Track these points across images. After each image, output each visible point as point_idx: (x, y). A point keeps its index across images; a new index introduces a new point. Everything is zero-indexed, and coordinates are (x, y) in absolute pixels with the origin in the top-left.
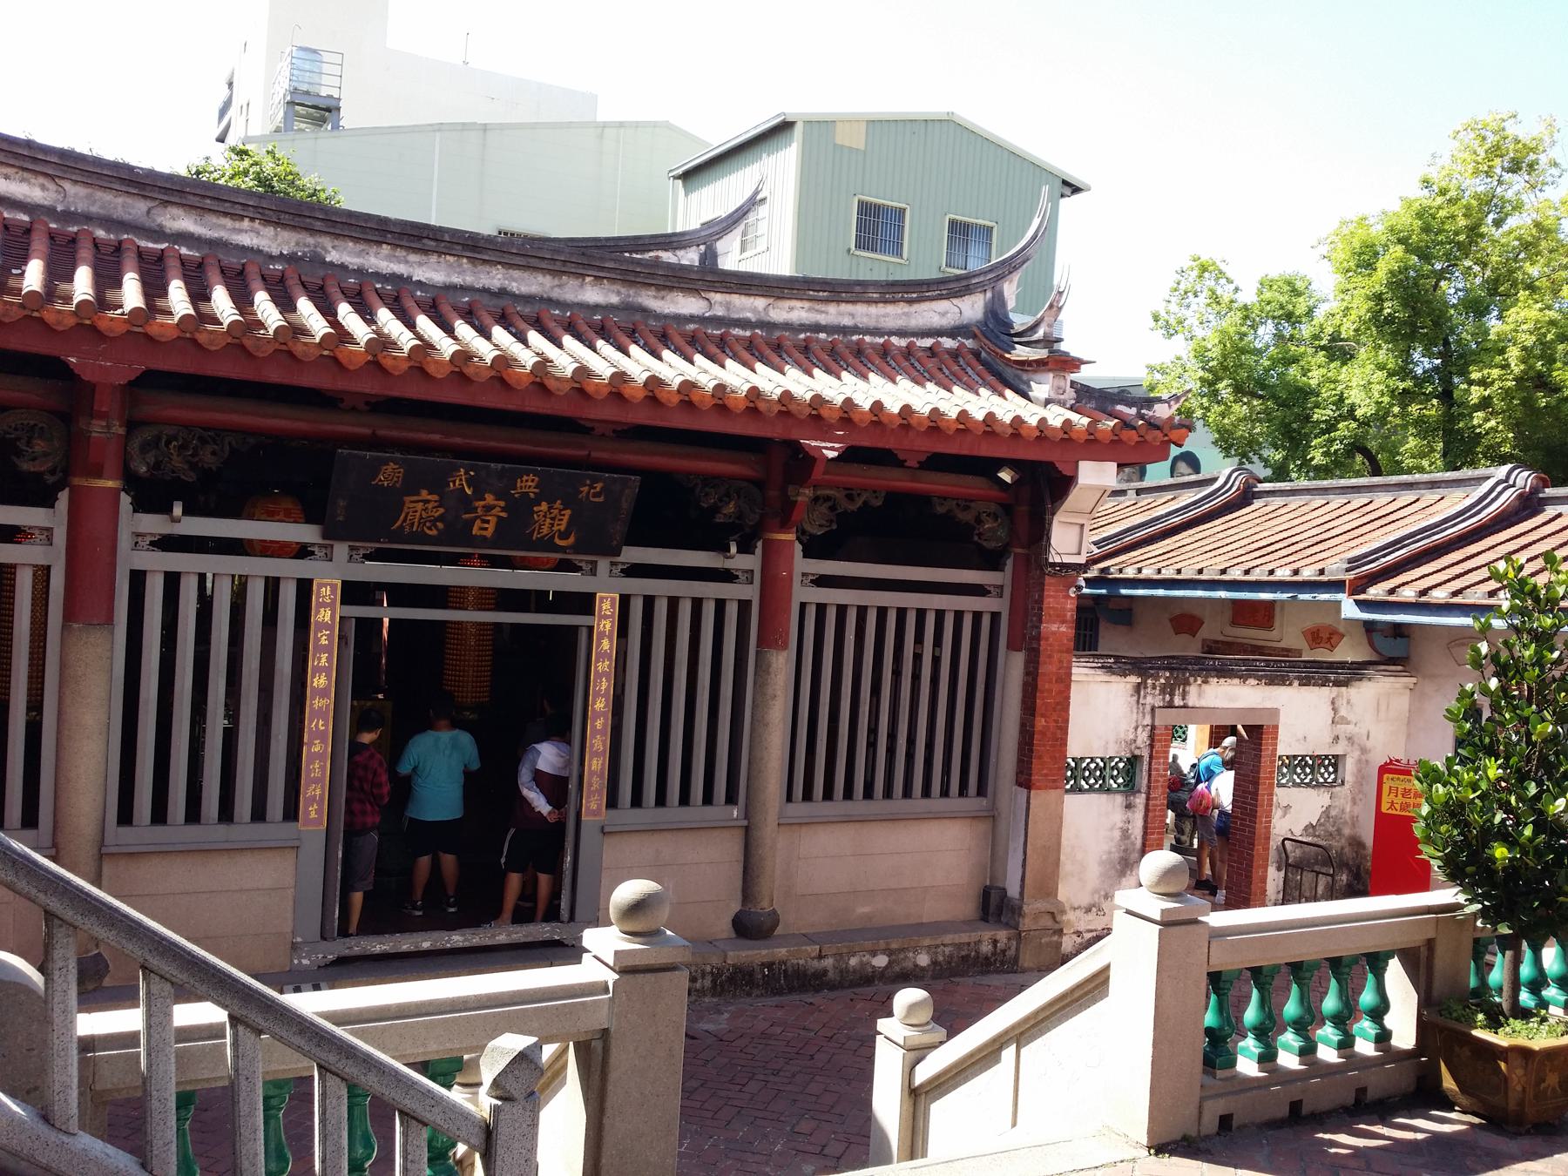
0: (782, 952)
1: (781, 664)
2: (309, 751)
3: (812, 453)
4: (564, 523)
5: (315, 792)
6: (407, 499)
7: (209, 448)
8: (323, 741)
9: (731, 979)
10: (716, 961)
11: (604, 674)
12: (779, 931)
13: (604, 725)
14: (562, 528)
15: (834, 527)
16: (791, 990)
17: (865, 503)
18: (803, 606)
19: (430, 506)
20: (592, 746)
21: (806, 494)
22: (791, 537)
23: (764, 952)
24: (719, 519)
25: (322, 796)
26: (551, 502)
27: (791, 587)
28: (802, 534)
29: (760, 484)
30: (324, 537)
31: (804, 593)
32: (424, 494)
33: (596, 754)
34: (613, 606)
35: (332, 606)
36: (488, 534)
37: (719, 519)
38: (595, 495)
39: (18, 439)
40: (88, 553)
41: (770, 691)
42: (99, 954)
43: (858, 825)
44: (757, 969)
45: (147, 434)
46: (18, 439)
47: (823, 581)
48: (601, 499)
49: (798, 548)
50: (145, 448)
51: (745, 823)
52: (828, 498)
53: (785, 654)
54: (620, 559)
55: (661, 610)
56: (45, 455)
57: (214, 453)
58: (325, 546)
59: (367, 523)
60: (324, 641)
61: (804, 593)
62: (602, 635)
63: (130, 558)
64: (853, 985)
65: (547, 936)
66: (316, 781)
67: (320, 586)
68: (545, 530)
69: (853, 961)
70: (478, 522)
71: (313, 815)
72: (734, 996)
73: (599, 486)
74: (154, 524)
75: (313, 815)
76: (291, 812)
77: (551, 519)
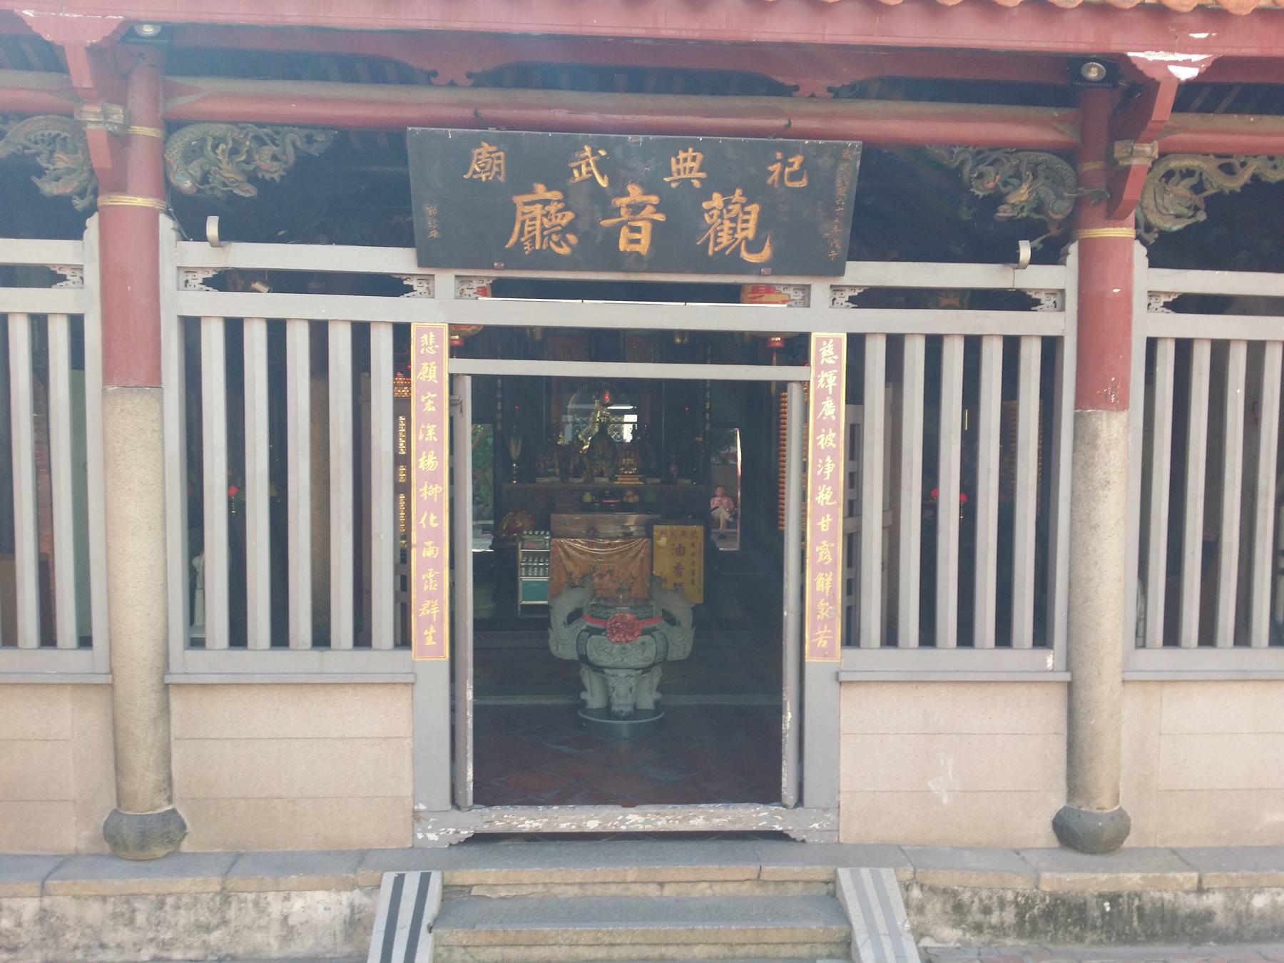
0: (1132, 880)
1: (1117, 434)
2: (419, 554)
3: (1150, 73)
4: (752, 225)
5: (431, 610)
6: (519, 200)
7: (268, 151)
8: (438, 543)
9: (1049, 914)
10: (1022, 885)
11: (829, 451)
12: (1129, 842)
13: (833, 526)
14: (750, 234)
15: (1202, 217)
16: (1151, 937)
17: (1255, 178)
18: (1152, 344)
19: (552, 208)
20: (815, 556)
21: (1142, 154)
22: (1125, 232)
23: (1103, 877)
24: (1004, 212)
25: (440, 615)
26: (727, 192)
27: (1129, 312)
28: (1144, 229)
29: (1069, 154)
30: (421, 264)
31: (1151, 322)
32: (541, 191)
33: (823, 568)
34: (837, 350)
35: (437, 358)
36: (643, 248)
37: (1004, 212)
38: (795, 176)
39: (38, 154)
40: (128, 294)
41: (1099, 475)
42: (174, 811)
43: (1261, 687)
44: (1092, 903)
45: (188, 136)
46: (38, 154)
47: (1184, 304)
48: (803, 183)
49: (1140, 252)
50: (191, 153)
51: (1067, 677)
52: (1189, 173)
53: (1123, 416)
54: (845, 280)
55: (915, 357)
56: (69, 171)
57: (275, 158)
58: (422, 278)
59: (474, 240)
60: (429, 408)
61: (1151, 322)
62: (822, 394)
63: (182, 299)
64: (1258, 937)
65: (762, 825)
66: (431, 596)
67: (422, 331)
68: (725, 239)
69: (1259, 902)
70: (624, 230)
71: (430, 641)
72: (1054, 940)
73: (797, 161)
74: (208, 255)
75: (430, 641)
76: (403, 639)
77: (731, 223)
